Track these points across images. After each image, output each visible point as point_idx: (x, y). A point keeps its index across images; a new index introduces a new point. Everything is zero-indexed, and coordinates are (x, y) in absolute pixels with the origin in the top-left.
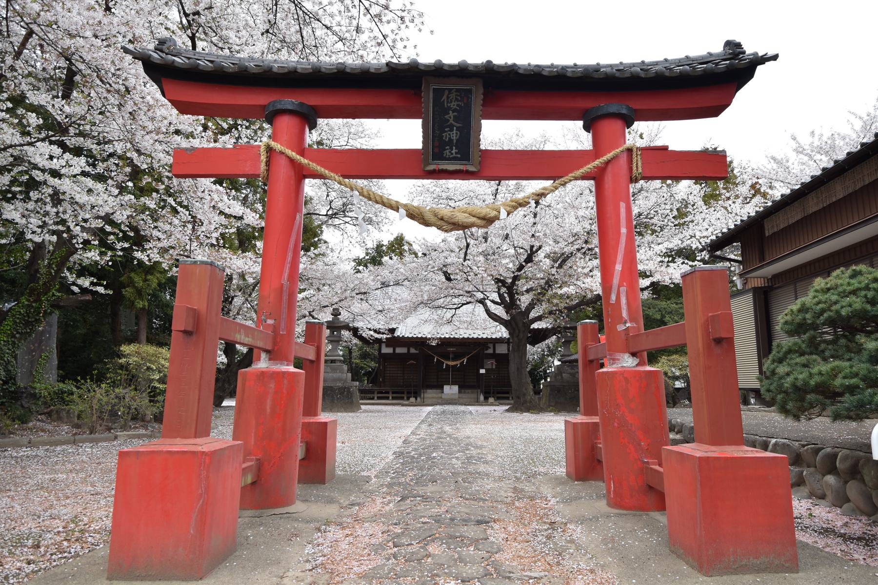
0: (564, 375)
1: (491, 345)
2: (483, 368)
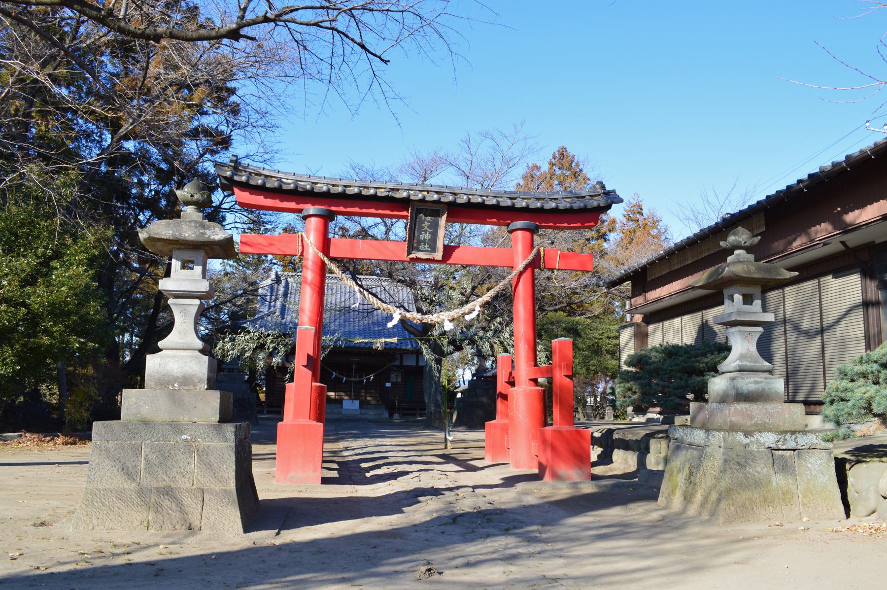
1: (398, 356)
2: (389, 382)
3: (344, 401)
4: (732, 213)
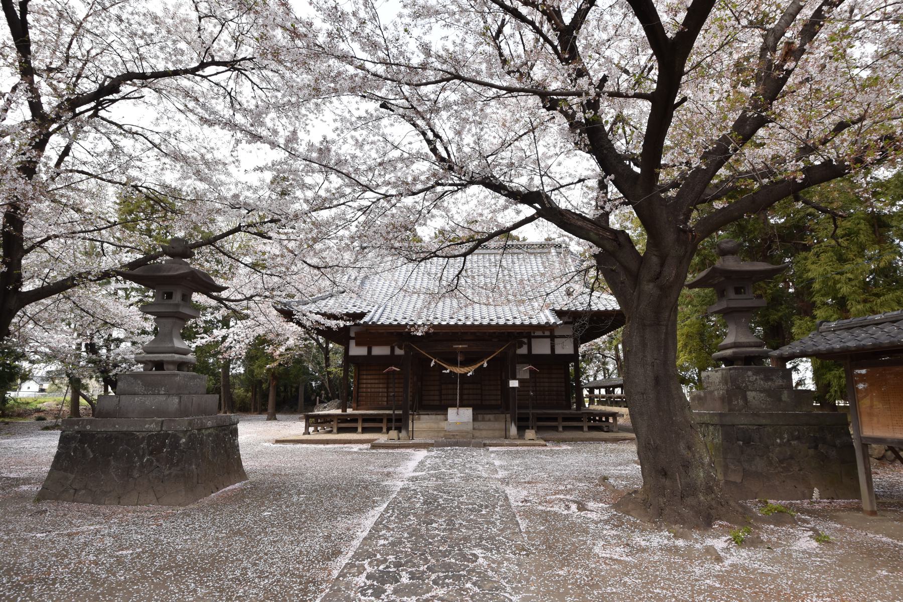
0: (751, 395)
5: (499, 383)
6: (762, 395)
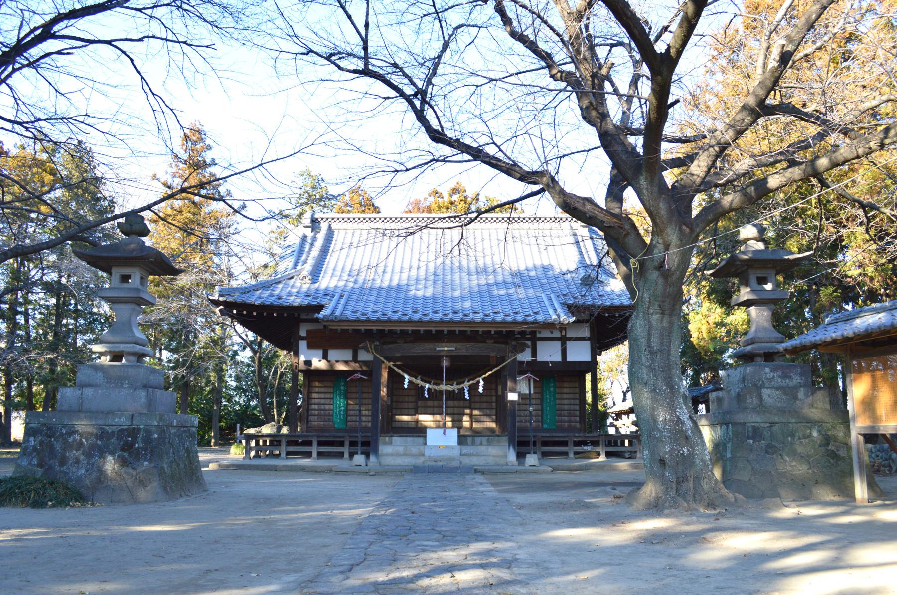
0: (766, 392)
3: (428, 431)
4: (671, 110)
5: (494, 399)
6: (778, 393)
